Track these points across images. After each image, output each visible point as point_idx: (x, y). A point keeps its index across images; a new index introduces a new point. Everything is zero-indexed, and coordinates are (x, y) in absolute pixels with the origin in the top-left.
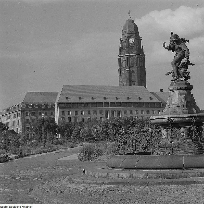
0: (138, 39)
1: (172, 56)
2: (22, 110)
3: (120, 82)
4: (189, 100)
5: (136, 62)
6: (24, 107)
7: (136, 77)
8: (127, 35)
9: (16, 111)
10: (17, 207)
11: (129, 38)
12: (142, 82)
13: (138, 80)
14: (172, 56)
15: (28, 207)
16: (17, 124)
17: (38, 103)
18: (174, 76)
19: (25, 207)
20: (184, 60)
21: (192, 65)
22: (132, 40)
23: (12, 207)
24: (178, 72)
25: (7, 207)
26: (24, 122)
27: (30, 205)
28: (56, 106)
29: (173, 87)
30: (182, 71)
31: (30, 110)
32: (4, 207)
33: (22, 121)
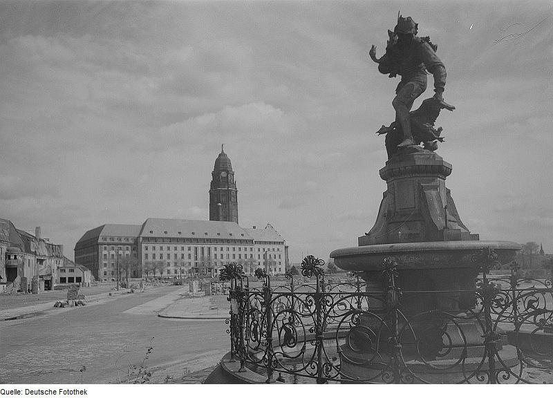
10: (47, 392)
15: (75, 392)
19: (68, 392)
21: (451, 109)
23: (32, 392)
25: (18, 392)
27: (80, 387)
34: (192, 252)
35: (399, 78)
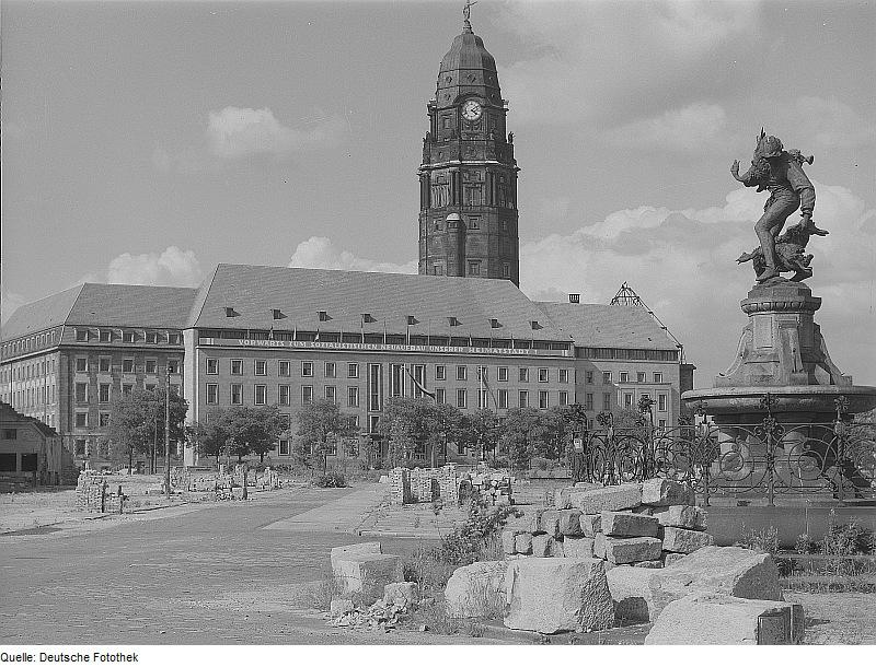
0: (495, 108)
1: (752, 204)
2: (65, 350)
3: (425, 260)
4: (808, 344)
5: (484, 191)
6: (70, 338)
7: (483, 242)
8: (455, 93)
9: (41, 355)
10: (74, 658)
11: (460, 102)
12: (505, 264)
13: (490, 258)
14: (752, 204)
15: (119, 657)
16: (41, 400)
17: (123, 328)
18: (760, 268)
19: (107, 658)
20: (795, 219)
21: (823, 234)
22: (472, 111)
23: (50, 658)
24: (776, 256)
25: (28, 658)
26: (68, 394)
27: (127, 650)
28: (189, 337)
29: (760, 300)
30: (788, 251)
31: (141, 352)
32: (19, 657)
33: (61, 390)
34: (362, 381)
35: (767, 194)
